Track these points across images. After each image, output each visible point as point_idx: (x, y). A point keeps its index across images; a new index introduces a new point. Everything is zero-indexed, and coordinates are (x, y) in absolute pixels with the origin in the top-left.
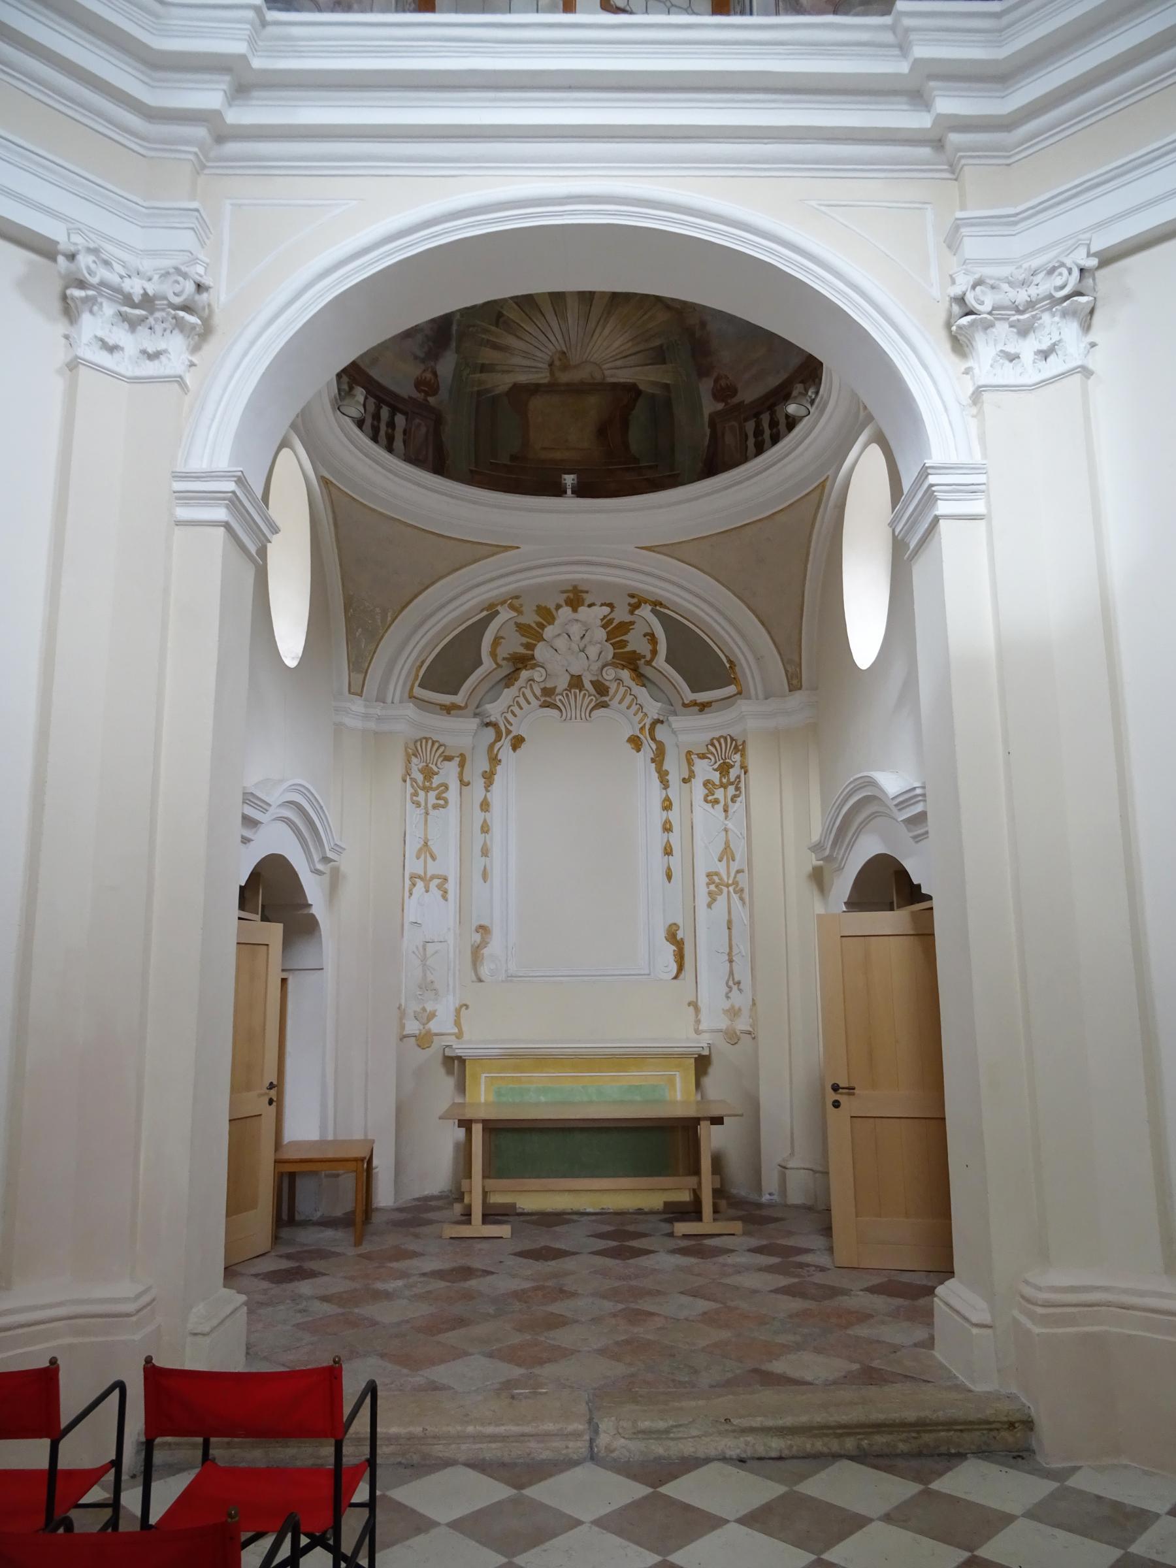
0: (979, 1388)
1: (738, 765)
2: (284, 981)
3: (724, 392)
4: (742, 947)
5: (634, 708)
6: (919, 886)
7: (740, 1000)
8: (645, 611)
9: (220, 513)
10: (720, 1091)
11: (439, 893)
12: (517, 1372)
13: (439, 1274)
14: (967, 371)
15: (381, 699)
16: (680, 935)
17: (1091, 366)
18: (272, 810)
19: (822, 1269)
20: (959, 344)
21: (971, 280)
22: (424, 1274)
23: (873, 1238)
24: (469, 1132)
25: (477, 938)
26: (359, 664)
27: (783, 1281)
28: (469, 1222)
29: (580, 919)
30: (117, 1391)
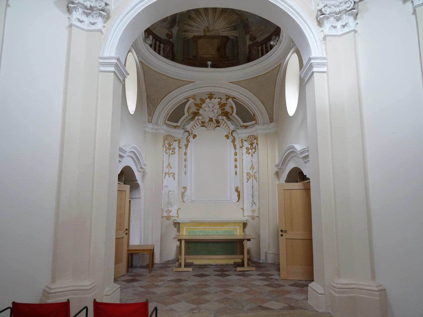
0: (320, 311)
1: (255, 143)
2: (130, 201)
3: (253, 39)
4: (256, 193)
5: (227, 127)
6: (306, 176)
7: (255, 208)
8: (230, 100)
9: (113, 69)
10: (249, 232)
11: (173, 178)
12: (194, 306)
13: (172, 281)
14: (322, 31)
15: (157, 124)
16: (239, 190)
17: (356, 30)
18: (127, 153)
19: (277, 280)
20: (320, 23)
21: (323, 5)
22: (168, 281)
23: (291, 271)
24: (181, 243)
25: (183, 190)
26: (151, 114)
27: (267, 283)
28: (181, 267)
29: (212, 185)
30: (85, 309)
